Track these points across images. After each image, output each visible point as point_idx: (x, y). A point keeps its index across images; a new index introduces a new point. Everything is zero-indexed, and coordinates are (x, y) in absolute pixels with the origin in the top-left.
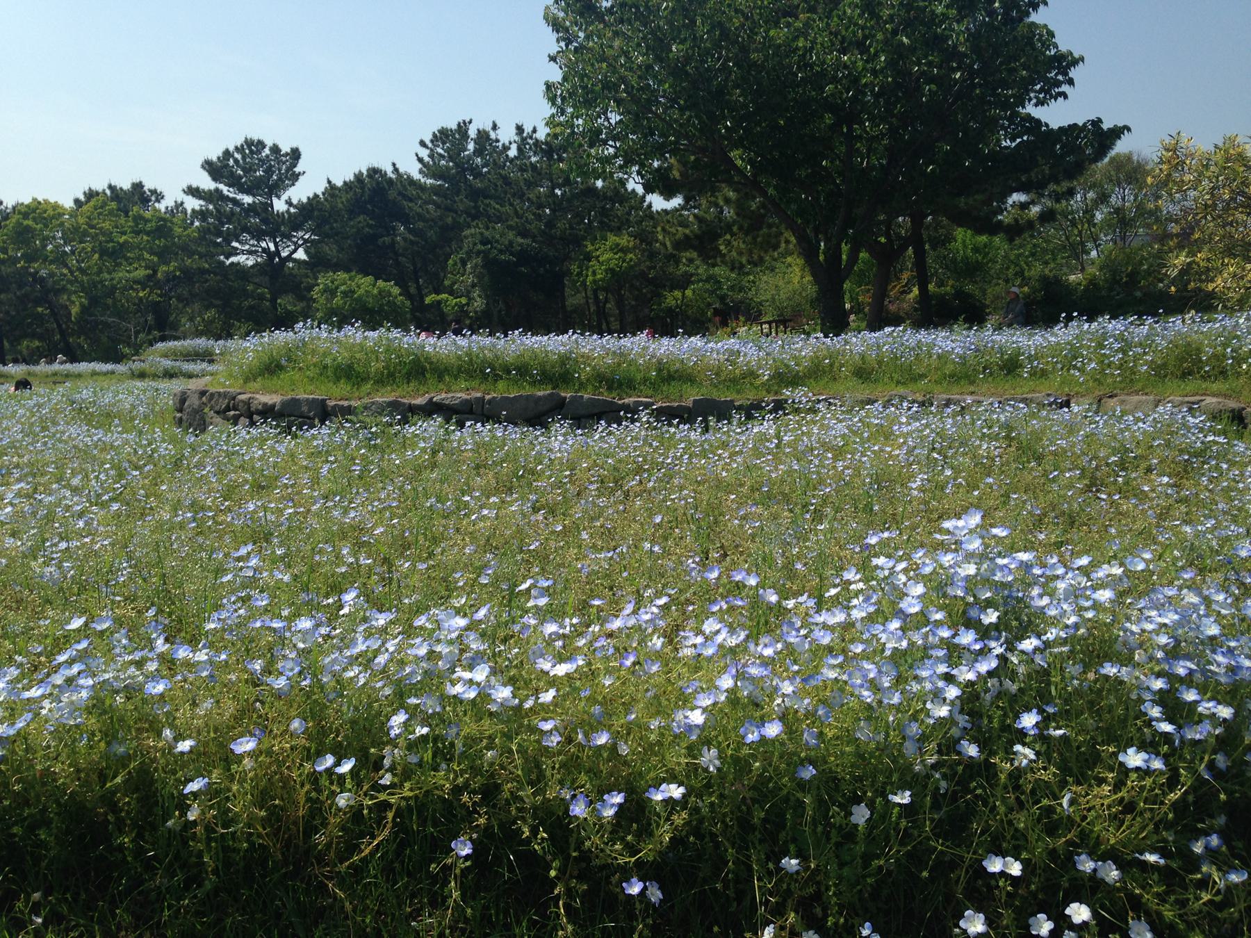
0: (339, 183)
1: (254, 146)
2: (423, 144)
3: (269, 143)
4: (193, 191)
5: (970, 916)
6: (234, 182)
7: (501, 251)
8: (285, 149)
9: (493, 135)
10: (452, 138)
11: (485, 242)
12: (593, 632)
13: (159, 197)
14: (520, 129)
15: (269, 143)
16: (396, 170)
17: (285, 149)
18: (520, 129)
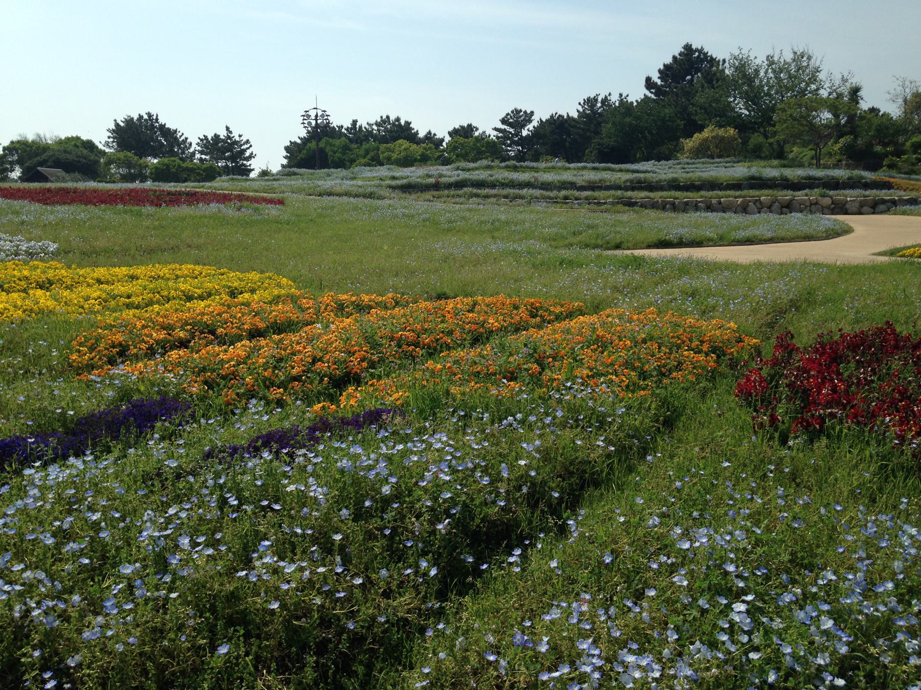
0: (544, 120)
1: (517, 112)
2: (580, 104)
3: (523, 110)
4: (496, 129)
5: (698, 181)
6: (510, 125)
7: (604, 148)
8: (528, 112)
9: (609, 98)
10: (591, 102)
11: (599, 144)
12: (153, 674)
13: (477, 129)
14: (621, 95)
15: (523, 110)
16: (568, 115)
17: (528, 112)
18: (621, 95)
